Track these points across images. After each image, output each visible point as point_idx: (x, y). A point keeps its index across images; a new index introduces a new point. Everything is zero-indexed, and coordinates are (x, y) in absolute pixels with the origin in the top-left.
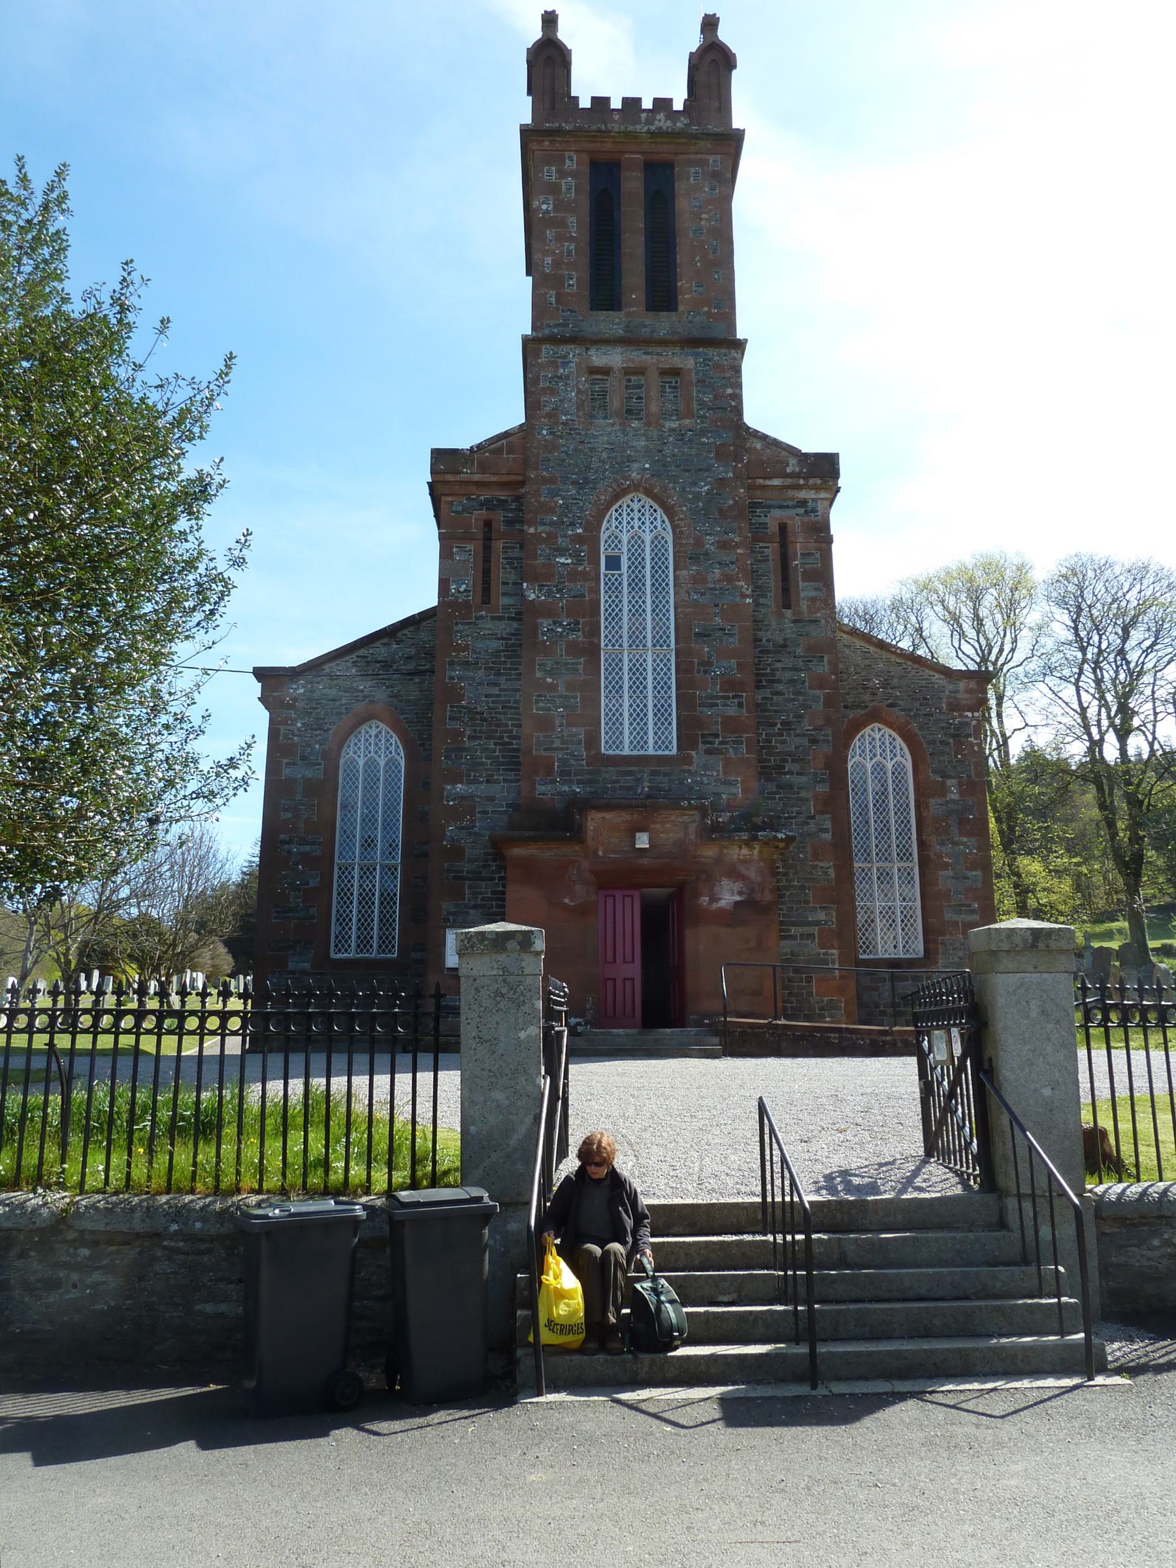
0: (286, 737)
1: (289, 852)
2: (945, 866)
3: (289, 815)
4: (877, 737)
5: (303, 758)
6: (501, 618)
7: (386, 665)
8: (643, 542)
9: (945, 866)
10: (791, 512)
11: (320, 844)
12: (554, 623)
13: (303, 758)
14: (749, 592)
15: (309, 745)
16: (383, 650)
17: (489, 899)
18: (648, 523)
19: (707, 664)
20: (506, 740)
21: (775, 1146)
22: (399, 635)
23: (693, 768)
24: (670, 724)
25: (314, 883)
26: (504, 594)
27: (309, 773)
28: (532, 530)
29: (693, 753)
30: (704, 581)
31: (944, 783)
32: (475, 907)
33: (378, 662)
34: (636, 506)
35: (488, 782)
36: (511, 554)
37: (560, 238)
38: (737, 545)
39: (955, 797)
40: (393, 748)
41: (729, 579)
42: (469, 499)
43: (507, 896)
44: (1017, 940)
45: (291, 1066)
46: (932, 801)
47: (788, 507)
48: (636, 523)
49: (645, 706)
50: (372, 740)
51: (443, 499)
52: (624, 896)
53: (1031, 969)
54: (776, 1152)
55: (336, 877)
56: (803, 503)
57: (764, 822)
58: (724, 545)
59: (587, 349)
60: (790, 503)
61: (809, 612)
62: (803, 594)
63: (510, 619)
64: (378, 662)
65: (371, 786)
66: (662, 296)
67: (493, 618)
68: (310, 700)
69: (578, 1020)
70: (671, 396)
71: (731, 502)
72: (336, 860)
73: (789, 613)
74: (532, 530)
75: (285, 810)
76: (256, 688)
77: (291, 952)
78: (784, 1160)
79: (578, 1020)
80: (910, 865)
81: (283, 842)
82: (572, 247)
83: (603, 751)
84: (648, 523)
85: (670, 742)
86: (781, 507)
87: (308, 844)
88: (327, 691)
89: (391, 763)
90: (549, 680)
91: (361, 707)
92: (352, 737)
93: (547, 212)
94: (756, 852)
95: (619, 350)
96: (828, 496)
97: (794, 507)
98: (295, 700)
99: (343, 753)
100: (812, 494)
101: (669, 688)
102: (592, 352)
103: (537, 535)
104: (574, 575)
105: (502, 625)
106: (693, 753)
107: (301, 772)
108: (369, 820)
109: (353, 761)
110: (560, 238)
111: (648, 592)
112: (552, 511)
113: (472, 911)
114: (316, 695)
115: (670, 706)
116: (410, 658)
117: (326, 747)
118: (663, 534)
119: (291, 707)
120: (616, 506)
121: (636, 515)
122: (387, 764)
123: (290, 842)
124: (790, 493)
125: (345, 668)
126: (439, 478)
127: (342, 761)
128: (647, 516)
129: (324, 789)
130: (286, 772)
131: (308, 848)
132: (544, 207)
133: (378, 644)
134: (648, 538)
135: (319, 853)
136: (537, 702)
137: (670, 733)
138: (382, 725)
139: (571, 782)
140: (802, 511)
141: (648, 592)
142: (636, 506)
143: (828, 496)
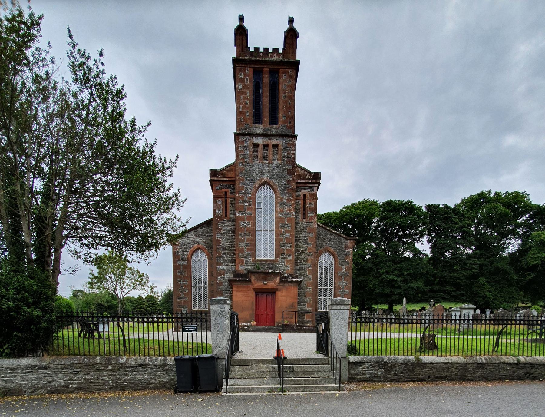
5: (182, 259)
9: (340, 289)
13: (182, 259)
25: (187, 291)
56: (310, 188)
66: (274, 120)
73: (304, 220)
91: (196, 246)
95: (261, 138)
104: (249, 209)
105: (230, 223)
112: (243, 189)
119: (178, 245)
129: (188, 267)
132: (240, 87)
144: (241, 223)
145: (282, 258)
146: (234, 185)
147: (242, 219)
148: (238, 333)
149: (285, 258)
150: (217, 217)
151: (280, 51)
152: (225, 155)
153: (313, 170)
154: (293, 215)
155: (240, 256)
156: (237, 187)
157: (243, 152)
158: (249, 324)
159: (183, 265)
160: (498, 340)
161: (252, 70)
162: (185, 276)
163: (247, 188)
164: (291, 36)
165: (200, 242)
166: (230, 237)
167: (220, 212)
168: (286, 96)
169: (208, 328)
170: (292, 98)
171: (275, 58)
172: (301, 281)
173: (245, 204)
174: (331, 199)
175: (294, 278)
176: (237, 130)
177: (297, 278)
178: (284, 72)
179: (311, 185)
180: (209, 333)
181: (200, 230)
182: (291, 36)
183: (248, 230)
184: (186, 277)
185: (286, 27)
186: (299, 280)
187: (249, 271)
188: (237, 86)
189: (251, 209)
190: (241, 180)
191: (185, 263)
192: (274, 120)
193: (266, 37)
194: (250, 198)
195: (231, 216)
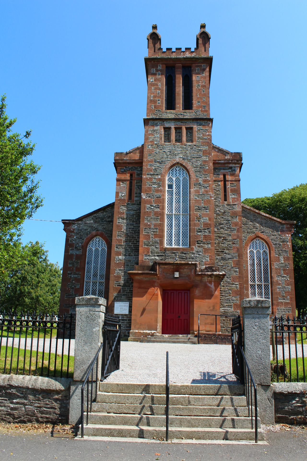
0: (71, 241)
1: (71, 277)
2: (279, 284)
3: (71, 265)
4: (258, 242)
5: (76, 248)
6: (134, 204)
7: (102, 219)
8: (173, 180)
9: (279, 284)
10: (227, 171)
11: (80, 275)
12: (151, 206)
13: (76, 248)
14: (213, 196)
15: (78, 244)
16: (101, 214)
17: (129, 293)
18: (181, 174)
19: (199, 219)
20: (135, 242)
21: (249, 376)
22: (106, 210)
23: (194, 252)
24: (187, 237)
25: (78, 287)
26: (136, 197)
27: (78, 253)
28: (145, 177)
29: (194, 247)
30: (199, 192)
31: (279, 257)
32: (124, 295)
33: (100, 218)
34: (178, 169)
35: (129, 255)
36: (138, 184)
37: (156, 89)
38: (209, 181)
39: (283, 262)
40: (103, 245)
41: (207, 192)
42: (126, 167)
43: (133, 292)
44: (252, 304)
45: (282, 359)
46: (275, 264)
47: (226, 169)
48: (178, 175)
49: (179, 232)
50: (97, 242)
51: (118, 167)
52: (179, 293)
53: (256, 313)
54: (250, 377)
55: (85, 285)
56: (231, 168)
57: (216, 269)
58: (205, 181)
59: (163, 122)
60: (227, 168)
61: (233, 202)
62: (230, 196)
63: (137, 204)
64: (100, 218)
65: (97, 256)
66: (188, 105)
67: (132, 204)
68: (78, 230)
69: (155, 331)
70: (189, 135)
71: (207, 168)
72: (85, 280)
73: (226, 202)
74: (145, 177)
75: (70, 264)
76: (62, 226)
77: (70, 308)
78: (252, 380)
79: (155, 331)
80: (267, 283)
81: (69, 274)
82: (160, 91)
83: (166, 246)
84: (181, 174)
85: (187, 243)
86: (224, 169)
87: (76, 274)
88: (84, 227)
89: (103, 250)
90: (149, 224)
91: (94, 233)
92: (91, 242)
93: (152, 81)
94: (213, 278)
95: (173, 122)
96: (239, 166)
97: (228, 169)
98: (74, 230)
99: (88, 246)
100: (234, 165)
101: (187, 226)
102: (165, 122)
103: (147, 178)
104: (157, 191)
105: (135, 206)
106: (194, 247)
107: (75, 252)
108: (96, 268)
109: (91, 249)
110: (156, 89)
111: (181, 196)
112: (151, 171)
113: (123, 296)
114: (80, 228)
115: (187, 232)
116: (110, 217)
117: (83, 244)
118: (186, 177)
119: (73, 232)
120: (172, 169)
121: (178, 172)
122: (102, 250)
123: (71, 274)
124: (226, 165)
125: (90, 221)
126: (117, 161)
127: (88, 249)
128: (181, 172)
129: (82, 258)
130: (71, 252)
131: (76, 276)
132: (151, 80)
133: (100, 213)
134: (181, 179)
135: (80, 277)
136: (145, 230)
137: (187, 240)
138: (100, 238)
139: (155, 256)
140: (230, 170)
141: (181, 196)
142: (178, 169)
143: (239, 166)
144: (148, 206)
145: (199, 247)
146: (141, 167)
147: (149, 202)
148: (118, 344)
149: (202, 246)
150: (120, 200)
151: (193, 50)
152: (131, 137)
153: (233, 150)
154: (211, 197)
155: (145, 244)
156: (144, 168)
157: (152, 135)
158: (153, 332)
159: (77, 255)
160: (70, 333)
161: (165, 66)
162: (76, 268)
163: (155, 169)
164: (204, 38)
165: (100, 228)
166: (133, 222)
167: (124, 194)
168: (199, 85)
169: (71, 336)
170: (207, 96)
171: (188, 55)
172: (224, 275)
173: (154, 186)
174: (258, 184)
175: (213, 271)
176: (147, 116)
177: (218, 270)
178: (197, 66)
179: (231, 165)
180: (73, 341)
181: (100, 215)
182: (204, 38)
183: (156, 214)
184: (78, 269)
185: (198, 31)
186: (221, 273)
187: (155, 264)
188: (149, 79)
189: (161, 191)
190: (149, 162)
191: (79, 253)
192: (188, 105)
193: (179, 39)
194: (160, 180)
195: (136, 199)
